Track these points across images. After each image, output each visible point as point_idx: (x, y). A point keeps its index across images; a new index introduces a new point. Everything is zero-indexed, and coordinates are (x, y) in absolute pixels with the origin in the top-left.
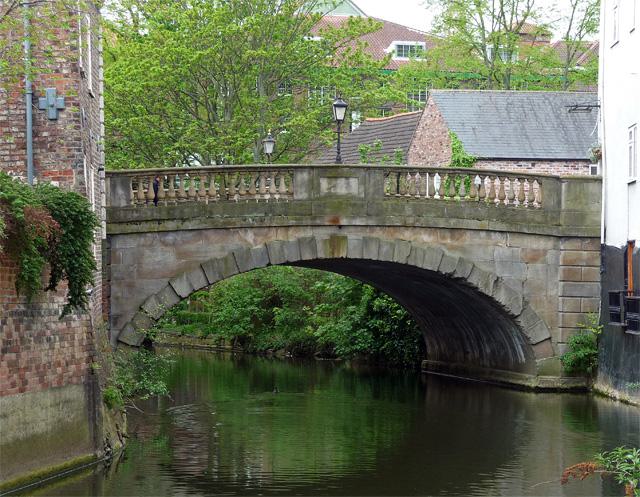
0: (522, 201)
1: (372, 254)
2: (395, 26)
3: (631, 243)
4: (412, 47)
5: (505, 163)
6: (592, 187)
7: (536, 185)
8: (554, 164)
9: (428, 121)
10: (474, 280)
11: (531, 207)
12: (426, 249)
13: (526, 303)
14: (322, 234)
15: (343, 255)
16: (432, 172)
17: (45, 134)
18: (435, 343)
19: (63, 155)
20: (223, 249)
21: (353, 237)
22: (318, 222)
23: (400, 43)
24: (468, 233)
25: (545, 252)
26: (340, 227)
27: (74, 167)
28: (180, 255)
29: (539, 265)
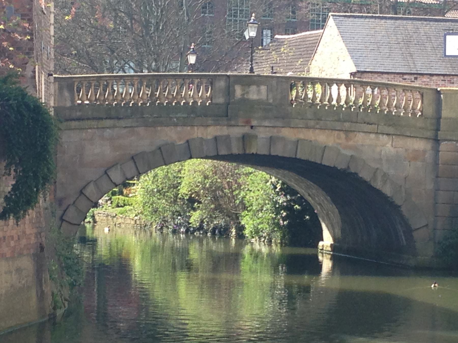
10: (365, 175)
14: (237, 132)
21: (263, 134)
22: (233, 123)
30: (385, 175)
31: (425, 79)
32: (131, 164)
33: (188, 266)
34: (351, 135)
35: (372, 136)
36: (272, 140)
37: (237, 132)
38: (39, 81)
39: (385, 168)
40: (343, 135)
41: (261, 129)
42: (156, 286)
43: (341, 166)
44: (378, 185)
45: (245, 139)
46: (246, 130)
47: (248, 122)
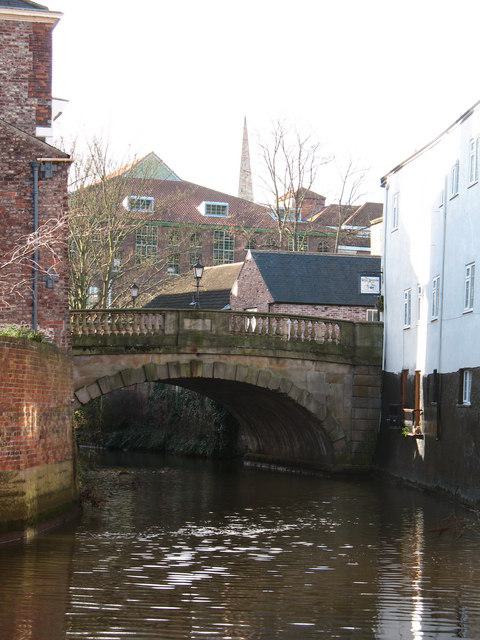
0: (333, 339)
1: (220, 375)
2: (219, 193)
3: (435, 371)
4: (219, 206)
5: (305, 306)
6: (376, 330)
7: (337, 327)
8: (342, 308)
9: (248, 273)
10: (293, 395)
11: (334, 343)
12: (254, 368)
13: (328, 412)
14: (184, 359)
15: (199, 374)
16: (250, 315)
17: (46, 297)
18: (254, 439)
19: (57, 311)
20: (113, 369)
21: (208, 360)
22: (182, 351)
23: (209, 203)
24: (288, 361)
25: (343, 375)
26: (198, 354)
27: (64, 319)
28: (82, 373)
29: (339, 385)
30: (309, 395)
31: (335, 309)
32: (95, 386)
33: (74, 341)
34: (281, 361)
35: (300, 362)
36: (215, 365)
37: (184, 359)
38: (86, 592)
39: (310, 389)
40: (274, 362)
41: (207, 357)
42: (26, 584)
43: (272, 386)
44: (304, 403)
45: (193, 364)
46: (194, 357)
47: (194, 351)
